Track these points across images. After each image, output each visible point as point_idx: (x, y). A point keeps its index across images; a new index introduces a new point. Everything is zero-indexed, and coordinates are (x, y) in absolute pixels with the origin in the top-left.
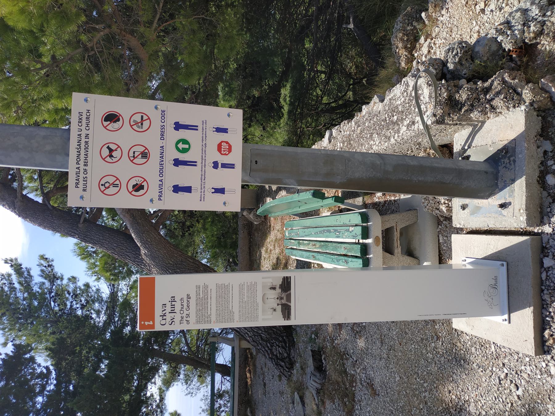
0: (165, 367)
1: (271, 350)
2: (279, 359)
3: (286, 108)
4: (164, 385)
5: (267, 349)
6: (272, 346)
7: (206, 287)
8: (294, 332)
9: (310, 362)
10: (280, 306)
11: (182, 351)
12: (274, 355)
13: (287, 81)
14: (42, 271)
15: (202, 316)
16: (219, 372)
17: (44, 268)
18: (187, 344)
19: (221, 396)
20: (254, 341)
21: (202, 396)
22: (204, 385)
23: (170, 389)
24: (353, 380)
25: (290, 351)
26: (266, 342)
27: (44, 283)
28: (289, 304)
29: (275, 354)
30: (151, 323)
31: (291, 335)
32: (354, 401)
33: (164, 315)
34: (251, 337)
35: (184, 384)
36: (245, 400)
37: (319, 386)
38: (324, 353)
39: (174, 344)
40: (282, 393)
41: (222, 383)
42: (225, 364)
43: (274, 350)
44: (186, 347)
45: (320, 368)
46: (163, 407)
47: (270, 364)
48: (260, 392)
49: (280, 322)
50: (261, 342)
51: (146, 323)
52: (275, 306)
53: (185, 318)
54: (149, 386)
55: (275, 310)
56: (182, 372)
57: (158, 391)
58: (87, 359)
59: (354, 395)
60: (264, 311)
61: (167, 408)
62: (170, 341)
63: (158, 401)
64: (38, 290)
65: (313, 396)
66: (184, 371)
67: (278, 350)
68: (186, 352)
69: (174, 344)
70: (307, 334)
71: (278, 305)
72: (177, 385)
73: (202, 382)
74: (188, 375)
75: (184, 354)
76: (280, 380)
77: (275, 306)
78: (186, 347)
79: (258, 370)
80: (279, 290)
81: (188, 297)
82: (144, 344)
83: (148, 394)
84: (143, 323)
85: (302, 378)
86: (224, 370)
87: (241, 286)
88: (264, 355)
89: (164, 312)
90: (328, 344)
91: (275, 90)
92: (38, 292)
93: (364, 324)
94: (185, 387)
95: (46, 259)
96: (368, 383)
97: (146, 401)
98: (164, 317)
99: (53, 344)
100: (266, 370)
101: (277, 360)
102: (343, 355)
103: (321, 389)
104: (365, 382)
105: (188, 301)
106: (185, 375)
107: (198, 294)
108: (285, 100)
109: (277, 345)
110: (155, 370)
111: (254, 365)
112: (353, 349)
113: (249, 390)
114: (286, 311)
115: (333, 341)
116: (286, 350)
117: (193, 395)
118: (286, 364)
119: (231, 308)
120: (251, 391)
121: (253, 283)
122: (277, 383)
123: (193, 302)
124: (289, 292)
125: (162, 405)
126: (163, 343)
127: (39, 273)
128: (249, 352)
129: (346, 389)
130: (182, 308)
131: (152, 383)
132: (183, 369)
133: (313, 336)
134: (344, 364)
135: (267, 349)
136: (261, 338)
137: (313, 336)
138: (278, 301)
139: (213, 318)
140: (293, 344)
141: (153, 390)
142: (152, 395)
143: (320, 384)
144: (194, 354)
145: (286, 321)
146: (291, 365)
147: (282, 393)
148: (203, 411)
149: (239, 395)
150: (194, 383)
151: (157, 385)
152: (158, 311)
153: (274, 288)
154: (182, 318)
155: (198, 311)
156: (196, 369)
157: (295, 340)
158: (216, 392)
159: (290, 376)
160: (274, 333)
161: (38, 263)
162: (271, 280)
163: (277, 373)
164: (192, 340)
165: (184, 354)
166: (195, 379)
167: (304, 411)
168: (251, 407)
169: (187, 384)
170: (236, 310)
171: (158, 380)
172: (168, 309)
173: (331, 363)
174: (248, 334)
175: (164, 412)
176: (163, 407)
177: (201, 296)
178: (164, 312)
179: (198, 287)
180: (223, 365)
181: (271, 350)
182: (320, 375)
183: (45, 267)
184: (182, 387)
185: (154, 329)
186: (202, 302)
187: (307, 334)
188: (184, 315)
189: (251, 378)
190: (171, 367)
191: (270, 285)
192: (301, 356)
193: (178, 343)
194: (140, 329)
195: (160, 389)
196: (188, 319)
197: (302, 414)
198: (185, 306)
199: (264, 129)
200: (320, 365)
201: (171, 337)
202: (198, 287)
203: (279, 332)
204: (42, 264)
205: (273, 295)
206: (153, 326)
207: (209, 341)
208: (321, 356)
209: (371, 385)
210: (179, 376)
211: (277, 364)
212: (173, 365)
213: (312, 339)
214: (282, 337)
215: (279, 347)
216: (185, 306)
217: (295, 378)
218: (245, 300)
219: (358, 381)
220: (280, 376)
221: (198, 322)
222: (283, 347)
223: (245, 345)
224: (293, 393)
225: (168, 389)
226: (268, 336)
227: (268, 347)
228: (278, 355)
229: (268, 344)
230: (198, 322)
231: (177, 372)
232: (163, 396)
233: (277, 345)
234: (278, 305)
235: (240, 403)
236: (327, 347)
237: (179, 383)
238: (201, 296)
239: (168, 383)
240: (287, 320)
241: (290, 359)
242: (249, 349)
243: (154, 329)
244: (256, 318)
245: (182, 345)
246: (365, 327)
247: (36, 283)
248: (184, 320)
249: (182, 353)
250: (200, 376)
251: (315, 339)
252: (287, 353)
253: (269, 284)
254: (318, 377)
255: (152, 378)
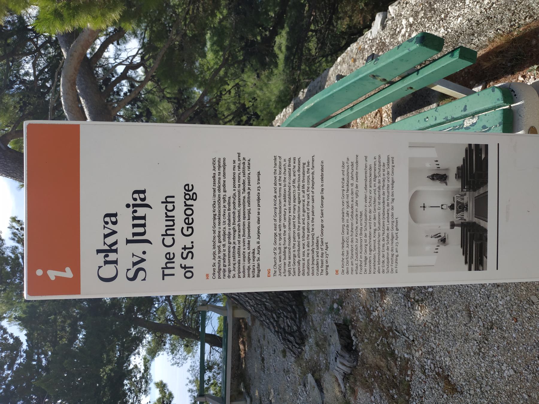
0: (149, 337)
1: (277, 322)
2: (287, 333)
3: (281, 57)
4: (149, 355)
5: (272, 320)
6: (278, 318)
7: (243, 164)
8: (306, 301)
9: (335, 339)
10: (458, 230)
11: (167, 320)
12: (281, 328)
13: (283, 28)
14: (14, 234)
15: (232, 253)
16: (208, 343)
17: (16, 231)
18: (173, 312)
19: (210, 368)
20: (256, 311)
21: (189, 367)
22: (190, 354)
23: (155, 359)
24: (406, 366)
25: (300, 323)
26: (271, 311)
27: (17, 248)
28: (482, 223)
29: (282, 326)
30: (68, 274)
31: (302, 303)
32: (409, 395)
33: (112, 249)
34: (252, 306)
35: (170, 353)
36: (239, 375)
37: (348, 370)
38: (354, 327)
39: (159, 313)
40: (287, 372)
41: (214, 355)
42: (213, 333)
43: (280, 322)
44: (172, 316)
45: (348, 347)
46: (148, 377)
47: (271, 336)
48: (257, 365)
49: (448, 271)
50: (264, 312)
51: (52, 274)
52: (444, 228)
53: (178, 260)
54: (132, 358)
55: (444, 241)
56: (168, 342)
57: (142, 361)
58: (63, 329)
59: (409, 386)
60: (412, 242)
61: (153, 378)
62: (155, 310)
63: (142, 371)
64: (11, 254)
65: (337, 380)
66: (170, 340)
67: (286, 323)
68: (172, 321)
69: (159, 313)
70: (325, 303)
71: (453, 225)
72: (163, 354)
73: (189, 352)
74: (174, 345)
75: (169, 323)
76: (284, 356)
77: (444, 228)
78: (172, 316)
79: (254, 342)
80: (454, 184)
81: (190, 194)
82: (126, 313)
83: (131, 367)
84: (39, 272)
85: (318, 356)
86: (214, 341)
87: (349, 169)
88: (269, 328)
89: (110, 240)
90: (360, 316)
91: (269, 41)
92: (10, 257)
93: (430, 290)
94: (171, 356)
95: (19, 221)
96: (438, 374)
97: (128, 374)
98: (112, 257)
99: (24, 312)
100: (263, 342)
101: (284, 334)
102: (388, 332)
103: (351, 374)
104: (432, 371)
105: (189, 207)
106: (171, 344)
107: (218, 186)
108: (280, 48)
109: (284, 316)
110: (138, 340)
111: (249, 337)
112: (407, 324)
113: (242, 363)
114: (475, 245)
115: (369, 313)
116: (295, 321)
117: (180, 365)
118: (294, 339)
119: (317, 233)
120: (245, 365)
121: (384, 160)
122: (280, 358)
123: (203, 210)
124: (481, 191)
125: (147, 375)
126: (147, 311)
127: (11, 236)
128: (243, 321)
129: (394, 377)
130: (170, 228)
131: (134, 355)
132: (169, 339)
133: (335, 306)
134: (389, 344)
135: (272, 320)
136: (266, 307)
137: (335, 306)
138: (453, 216)
139: (267, 260)
140: (304, 315)
141: (136, 361)
142: (136, 367)
143: (350, 367)
144: (180, 323)
145: (473, 272)
146: (302, 340)
147: (287, 372)
148: (190, 382)
149: (232, 368)
150: (180, 353)
151: (141, 355)
152: (91, 236)
153: (440, 177)
154: (170, 258)
155: (219, 237)
156: (183, 339)
157: (307, 310)
158: (206, 364)
159: (300, 353)
160: (281, 302)
161: (9, 225)
162: (432, 154)
163: (280, 346)
164: (178, 308)
165: (169, 323)
166: (182, 349)
167: (322, 398)
168: (244, 381)
169: (173, 353)
170: (333, 236)
171: (143, 351)
172: (125, 228)
173: (366, 341)
174: (249, 303)
175: (149, 381)
176: (148, 377)
177: (230, 192)
178: (110, 240)
179: (219, 164)
180: (211, 335)
181: (277, 322)
182: (350, 357)
183: (17, 229)
184: (168, 357)
185: (79, 293)
186: (233, 211)
187: (325, 303)
188: (177, 250)
189: (245, 350)
190: (156, 336)
191: (430, 167)
192: (315, 330)
193: (164, 311)
194: (29, 293)
195: (145, 359)
196: (188, 262)
197: (320, 401)
198: (180, 223)
199: (258, 76)
200: (348, 343)
201: (156, 305)
202: (219, 164)
203: (287, 300)
204: (13, 227)
205: (439, 195)
206: (74, 284)
207: (197, 308)
208: (349, 331)
209: (444, 377)
210: (164, 345)
211: (284, 339)
212: (158, 334)
213: (333, 308)
214: (291, 306)
215: (287, 318)
216: (180, 223)
217: (307, 356)
218: (361, 208)
219: (416, 368)
220: (284, 352)
221: (219, 272)
222: (292, 319)
223: (240, 313)
224: (304, 374)
225: (153, 358)
226: (274, 305)
227: (274, 318)
228: (286, 328)
229: (274, 316)
230: (219, 272)
231: (162, 341)
232: (148, 365)
233: (284, 316)
234: (453, 225)
235: (233, 377)
236: (358, 320)
237: (165, 353)
238: (230, 192)
239: (153, 353)
240: (477, 269)
241: (300, 332)
242: (243, 319)
243: (79, 293)
244: (390, 263)
245: (168, 313)
246: (432, 294)
247: (7, 248)
248: (177, 265)
249: (167, 322)
250: (187, 346)
251: (338, 309)
252: (297, 326)
253: (428, 165)
254: (347, 359)
255: (136, 349)
